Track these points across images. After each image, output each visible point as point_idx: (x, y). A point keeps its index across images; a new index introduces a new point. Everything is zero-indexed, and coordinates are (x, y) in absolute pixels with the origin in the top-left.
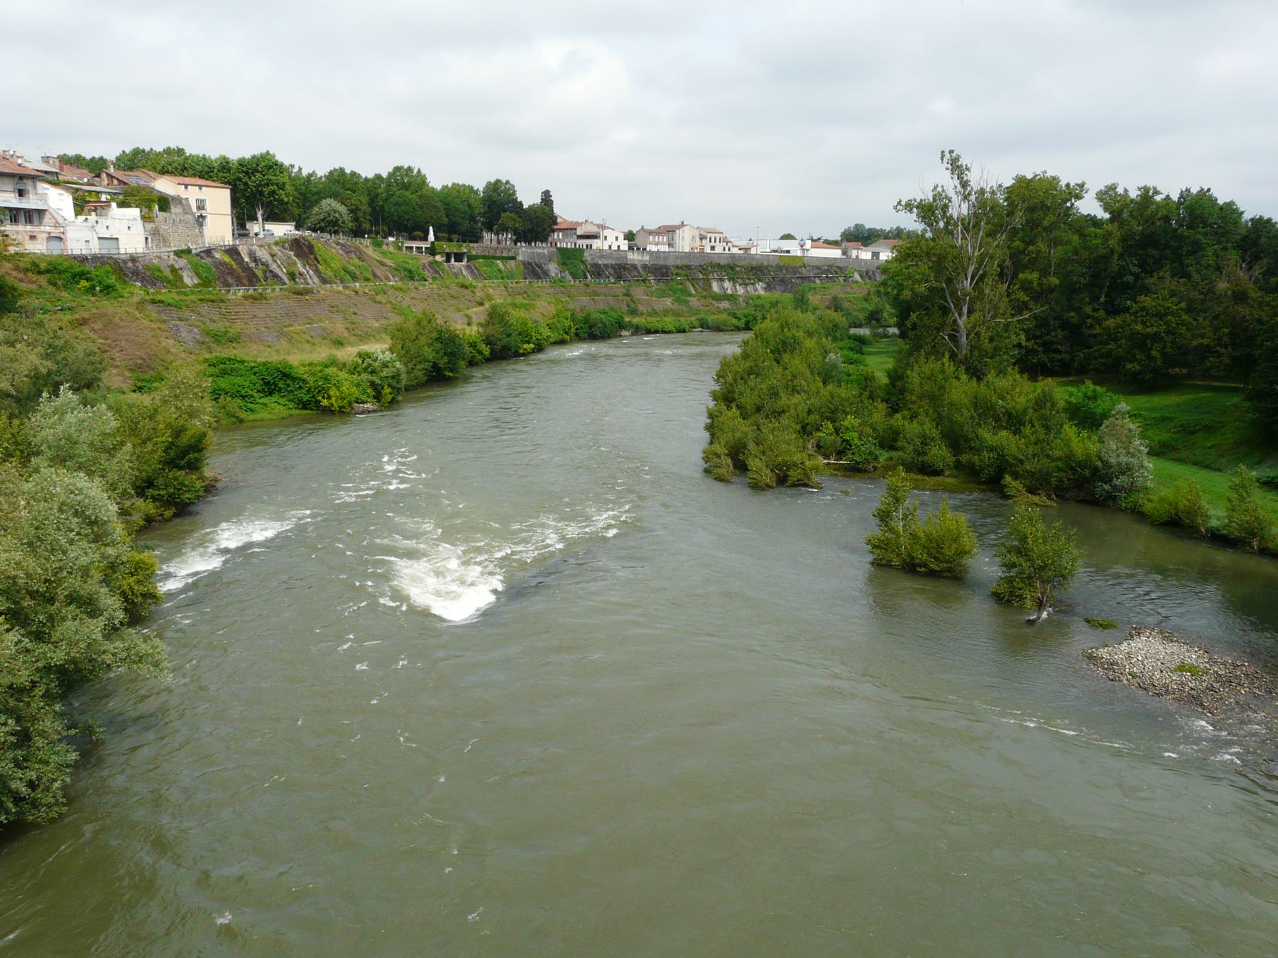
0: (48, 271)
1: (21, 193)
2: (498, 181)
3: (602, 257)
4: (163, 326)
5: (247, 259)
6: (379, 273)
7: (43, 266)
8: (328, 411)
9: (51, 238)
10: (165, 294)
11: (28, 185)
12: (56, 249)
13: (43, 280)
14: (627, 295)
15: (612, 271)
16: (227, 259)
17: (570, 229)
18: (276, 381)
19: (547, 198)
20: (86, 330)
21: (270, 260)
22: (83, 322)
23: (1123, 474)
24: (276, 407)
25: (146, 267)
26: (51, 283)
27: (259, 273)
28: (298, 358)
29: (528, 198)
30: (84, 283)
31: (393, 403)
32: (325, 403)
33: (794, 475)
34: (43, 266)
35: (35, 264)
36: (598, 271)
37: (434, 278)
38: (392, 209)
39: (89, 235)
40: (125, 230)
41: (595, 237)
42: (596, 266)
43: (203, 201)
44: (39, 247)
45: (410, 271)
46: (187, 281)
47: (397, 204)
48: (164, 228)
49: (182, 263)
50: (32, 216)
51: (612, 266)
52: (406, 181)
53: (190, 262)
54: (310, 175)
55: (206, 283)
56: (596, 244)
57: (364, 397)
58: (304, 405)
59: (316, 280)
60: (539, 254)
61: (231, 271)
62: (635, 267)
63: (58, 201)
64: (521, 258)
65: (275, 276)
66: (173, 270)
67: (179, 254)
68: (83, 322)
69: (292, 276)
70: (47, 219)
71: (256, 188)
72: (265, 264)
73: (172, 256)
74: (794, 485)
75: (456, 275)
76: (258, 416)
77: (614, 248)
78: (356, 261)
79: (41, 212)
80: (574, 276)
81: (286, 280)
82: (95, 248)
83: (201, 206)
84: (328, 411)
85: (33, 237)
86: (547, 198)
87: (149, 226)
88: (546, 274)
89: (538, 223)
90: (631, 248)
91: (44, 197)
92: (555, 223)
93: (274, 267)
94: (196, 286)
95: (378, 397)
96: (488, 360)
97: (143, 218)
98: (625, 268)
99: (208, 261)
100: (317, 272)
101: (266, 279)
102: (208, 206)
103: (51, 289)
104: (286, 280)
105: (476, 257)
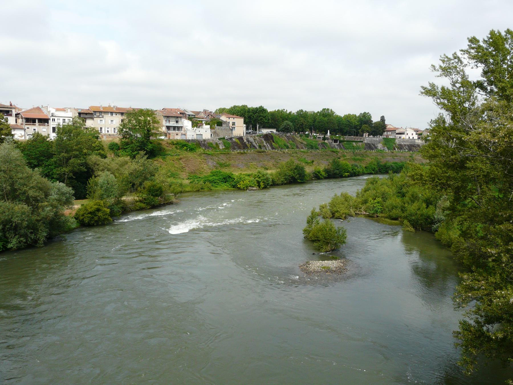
0: (176, 144)
1: (177, 122)
2: (365, 113)
3: (404, 141)
4: (205, 161)
5: (245, 141)
6: (299, 146)
7: (175, 142)
8: (239, 189)
9: (182, 134)
10: (210, 152)
11: (179, 119)
12: (184, 138)
13: (174, 147)
14: (410, 157)
15: (407, 147)
16: (237, 141)
17: (393, 131)
18: (227, 179)
19: (383, 119)
20: (181, 161)
21: (253, 141)
22: (181, 159)
23: (439, 222)
24: (225, 186)
25: (208, 143)
26: (176, 148)
27: (249, 146)
28: (236, 174)
29: (375, 119)
30: (185, 148)
31: (265, 188)
32: (239, 186)
33: (337, 215)
34: (175, 142)
35: (173, 142)
36: (401, 147)
37: (322, 149)
38: (324, 124)
39: (193, 133)
40: (205, 133)
41: (403, 134)
42: (400, 145)
43: (234, 123)
44: (179, 138)
45: (312, 146)
46: (221, 147)
47: (319, 122)
48: (218, 131)
49: (221, 142)
50: (179, 128)
51: (408, 145)
52: (326, 114)
53: (223, 142)
54: (290, 113)
55: (227, 148)
56: (403, 136)
57: (253, 185)
58: (234, 186)
59: (270, 148)
60: (374, 140)
61: (241, 144)
62: (419, 146)
63: (187, 124)
64: (366, 142)
65: (254, 146)
66: (217, 144)
67: (220, 139)
68: (181, 159)
69: (260, 147)
70: (183, 129)
71: (255, 118)
72: (252, 143)
73: (217, 140)
74: (337, 218)
75: (332, 148)
76: (217, 189)
77: (411, 138)
78: (291, 142)
79: (182, 127)
80: (389, 149)
81: (258, 148)
82: (195, 137)
83: (234, 124)
84: (239, 189)
85: (177, 134)
86: (383, 119)
87: (213, 131)
88: (376, 148)
89: (380, 128)
90: (419, 138)
91: (183, 123)
92: (385, 128)
93: (254, 144)
94: (223, 149)
95: (259, 186)
96: (326, 178)
97: (211, 128)
98: (414, 146)
99: (230, 141)
100: (271, 145)
101: (251, 147)
102: (236, 124)
103: (175, 149)
104: (258, 148)
105: (343, 141)
